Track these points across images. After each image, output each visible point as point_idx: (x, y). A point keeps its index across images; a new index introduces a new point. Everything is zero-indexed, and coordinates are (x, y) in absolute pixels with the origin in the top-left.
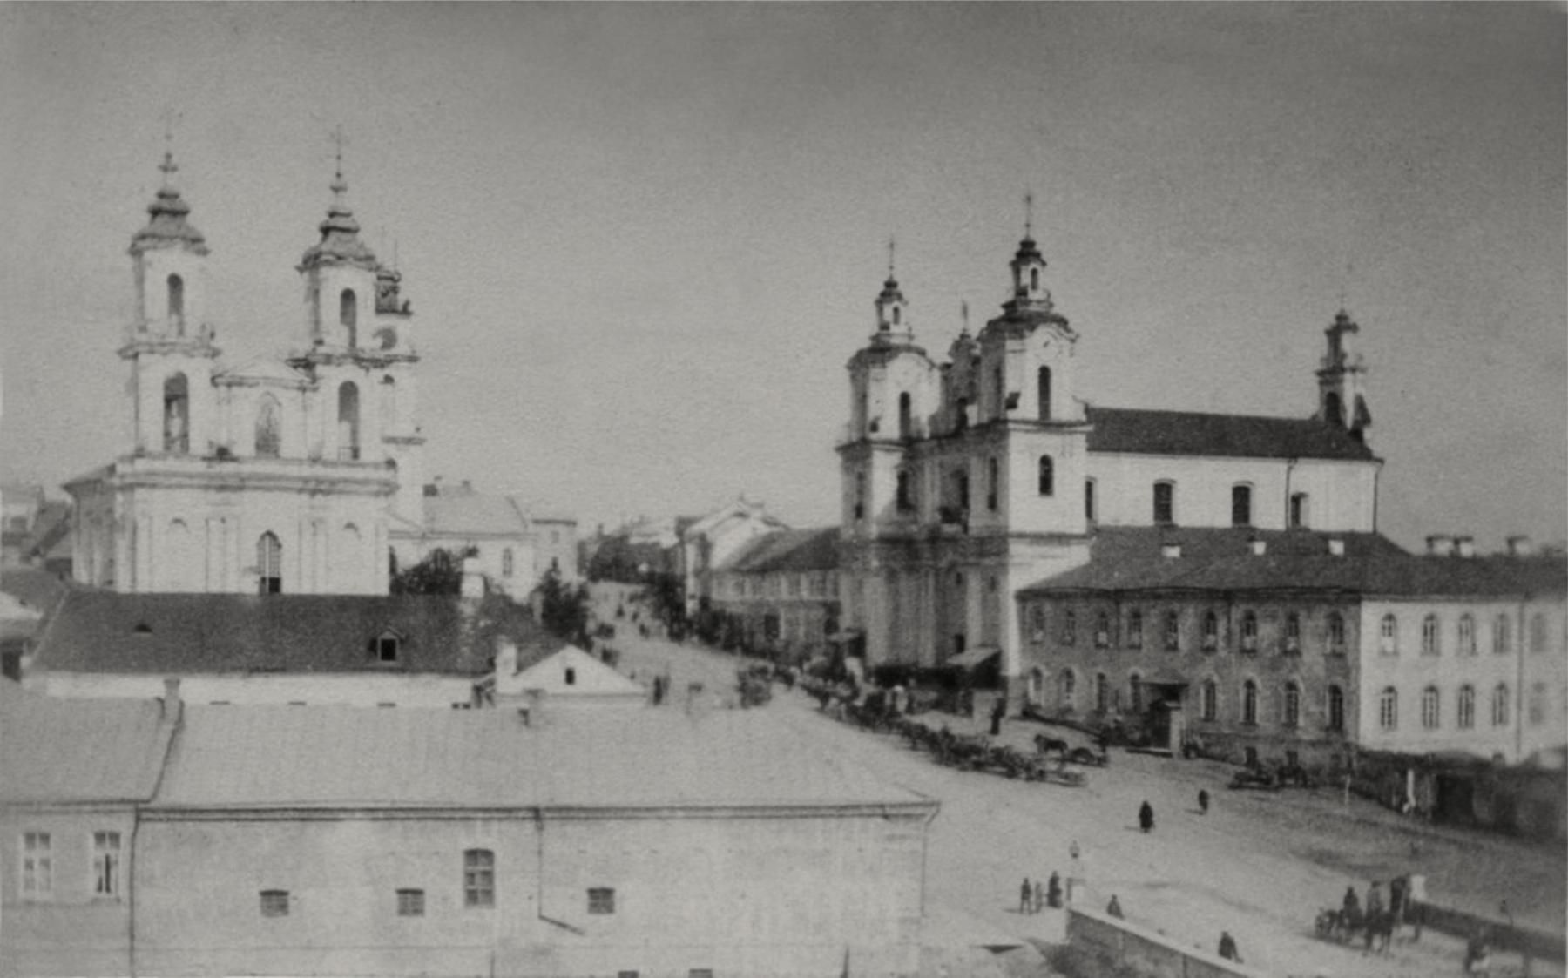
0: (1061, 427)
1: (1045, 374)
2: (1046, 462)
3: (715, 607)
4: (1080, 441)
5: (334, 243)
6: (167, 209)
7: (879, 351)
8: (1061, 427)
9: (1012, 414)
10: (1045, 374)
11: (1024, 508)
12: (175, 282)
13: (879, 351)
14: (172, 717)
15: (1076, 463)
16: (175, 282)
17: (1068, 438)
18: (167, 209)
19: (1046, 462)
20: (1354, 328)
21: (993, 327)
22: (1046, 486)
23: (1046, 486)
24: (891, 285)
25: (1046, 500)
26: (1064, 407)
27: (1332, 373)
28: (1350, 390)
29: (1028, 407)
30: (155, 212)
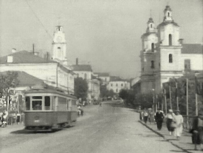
2: (170, 56)
8: (176, 47)
10: (170, 36)
11: (165, 65)
15: (180, 60)
22: (171, 60)
23: (171, 60)
29: (166, 42)
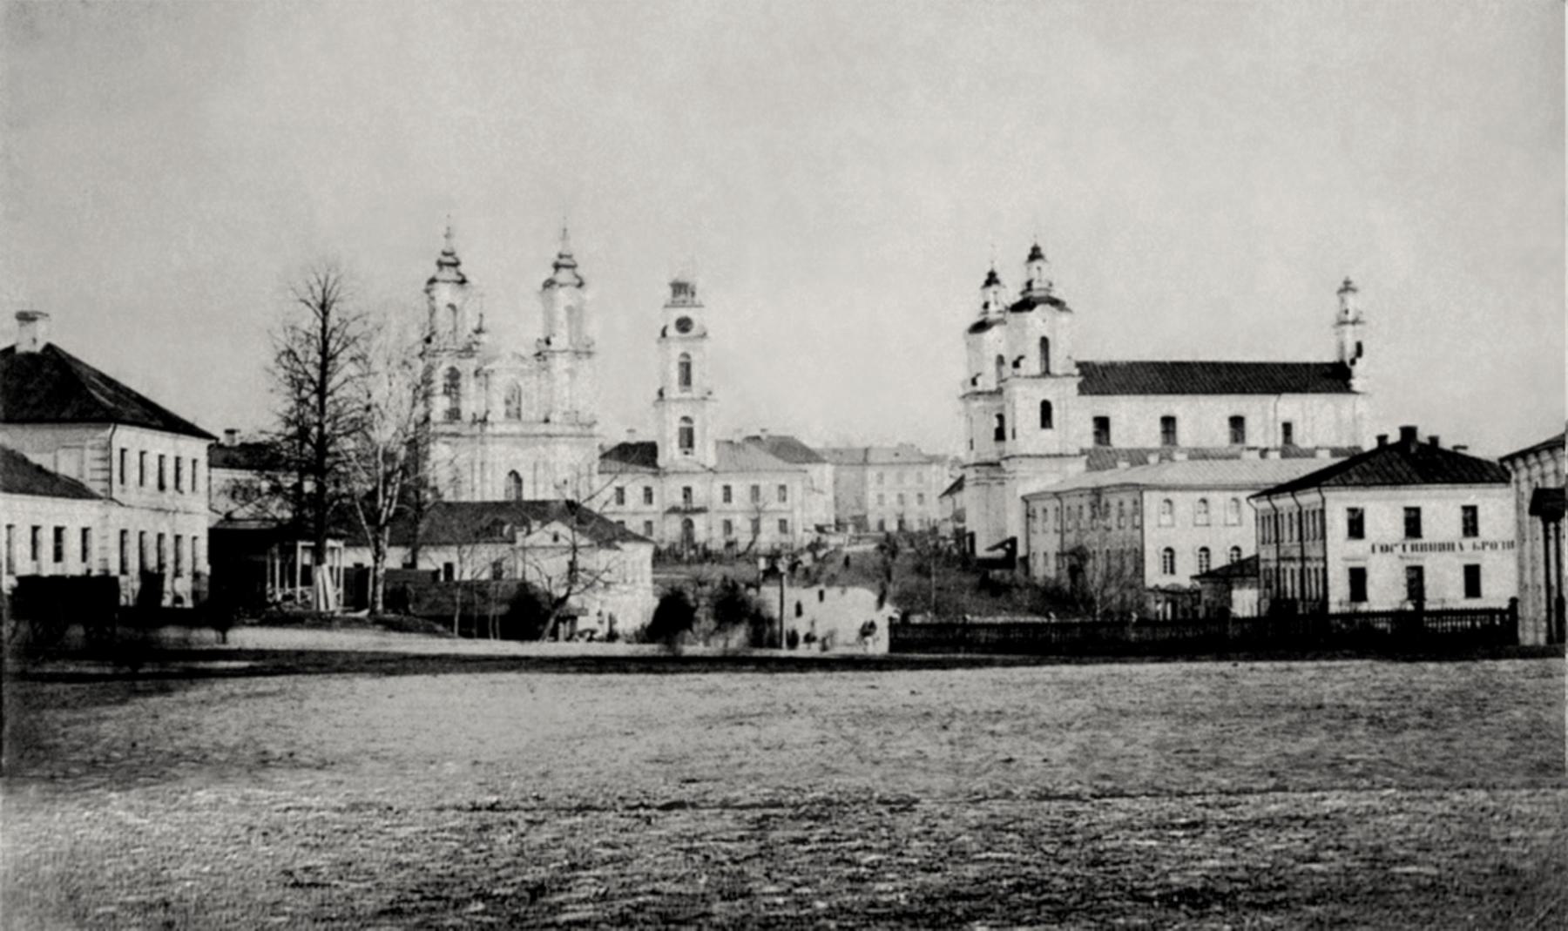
2: (1046, 408)
5: (564, 275)
15: (1076, 413)
18: (449, 261)
19: (1046, 408)
26: (1058, 363)
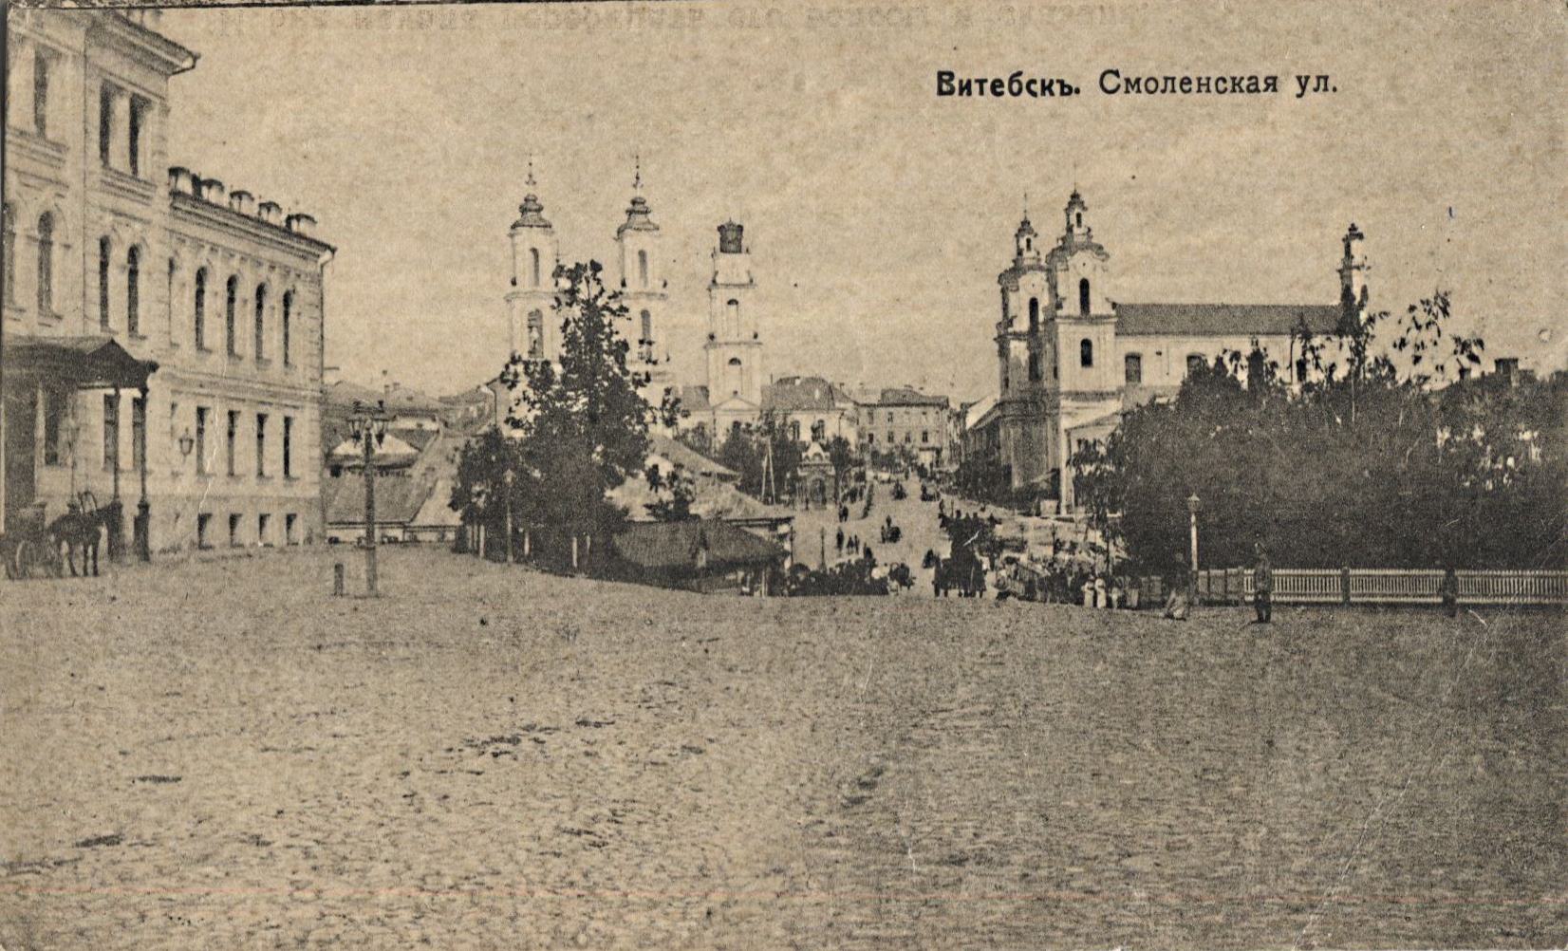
0: (1098, 320)
1: (1084, 285)
2: (1086, 344)
3: (343, 398)
4: (1111, 329)
5: (638, 207)
6: (637, 207)
7: (1017, 270)
8: (1098, 320)
9: (1059, 312)
10: (1084, 285)
11: (1071, 375)
12: (642, 254)
13: (1017, 270)
14: (1345, 579)
16: (642, 254)
17: (1102, 328)
19: (1086, 344)
20: (1360, 236)
21: (1052, 254)
22: (1087, 361)
23: (1087, 361)
24: (1025, 223)
25: (1087, 370)
26: (1097, 307)
27: (1345, 271)
28: (1357, 282)
29: (1072, 306)
30: (630, 212)
